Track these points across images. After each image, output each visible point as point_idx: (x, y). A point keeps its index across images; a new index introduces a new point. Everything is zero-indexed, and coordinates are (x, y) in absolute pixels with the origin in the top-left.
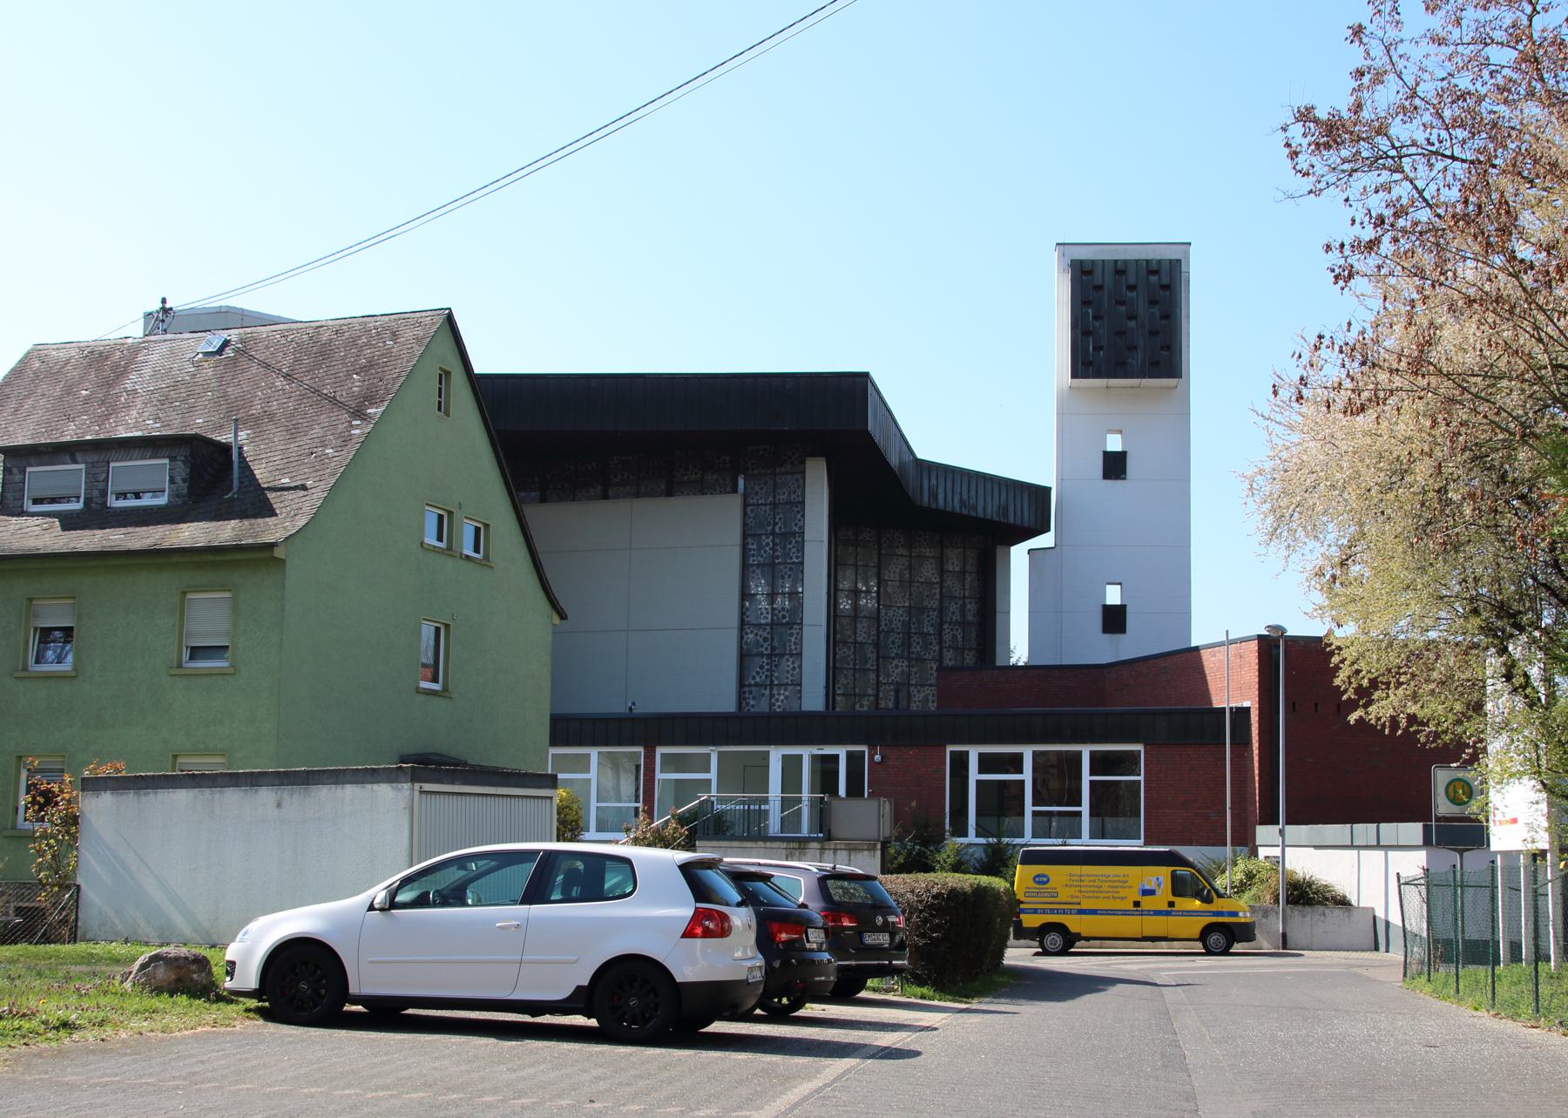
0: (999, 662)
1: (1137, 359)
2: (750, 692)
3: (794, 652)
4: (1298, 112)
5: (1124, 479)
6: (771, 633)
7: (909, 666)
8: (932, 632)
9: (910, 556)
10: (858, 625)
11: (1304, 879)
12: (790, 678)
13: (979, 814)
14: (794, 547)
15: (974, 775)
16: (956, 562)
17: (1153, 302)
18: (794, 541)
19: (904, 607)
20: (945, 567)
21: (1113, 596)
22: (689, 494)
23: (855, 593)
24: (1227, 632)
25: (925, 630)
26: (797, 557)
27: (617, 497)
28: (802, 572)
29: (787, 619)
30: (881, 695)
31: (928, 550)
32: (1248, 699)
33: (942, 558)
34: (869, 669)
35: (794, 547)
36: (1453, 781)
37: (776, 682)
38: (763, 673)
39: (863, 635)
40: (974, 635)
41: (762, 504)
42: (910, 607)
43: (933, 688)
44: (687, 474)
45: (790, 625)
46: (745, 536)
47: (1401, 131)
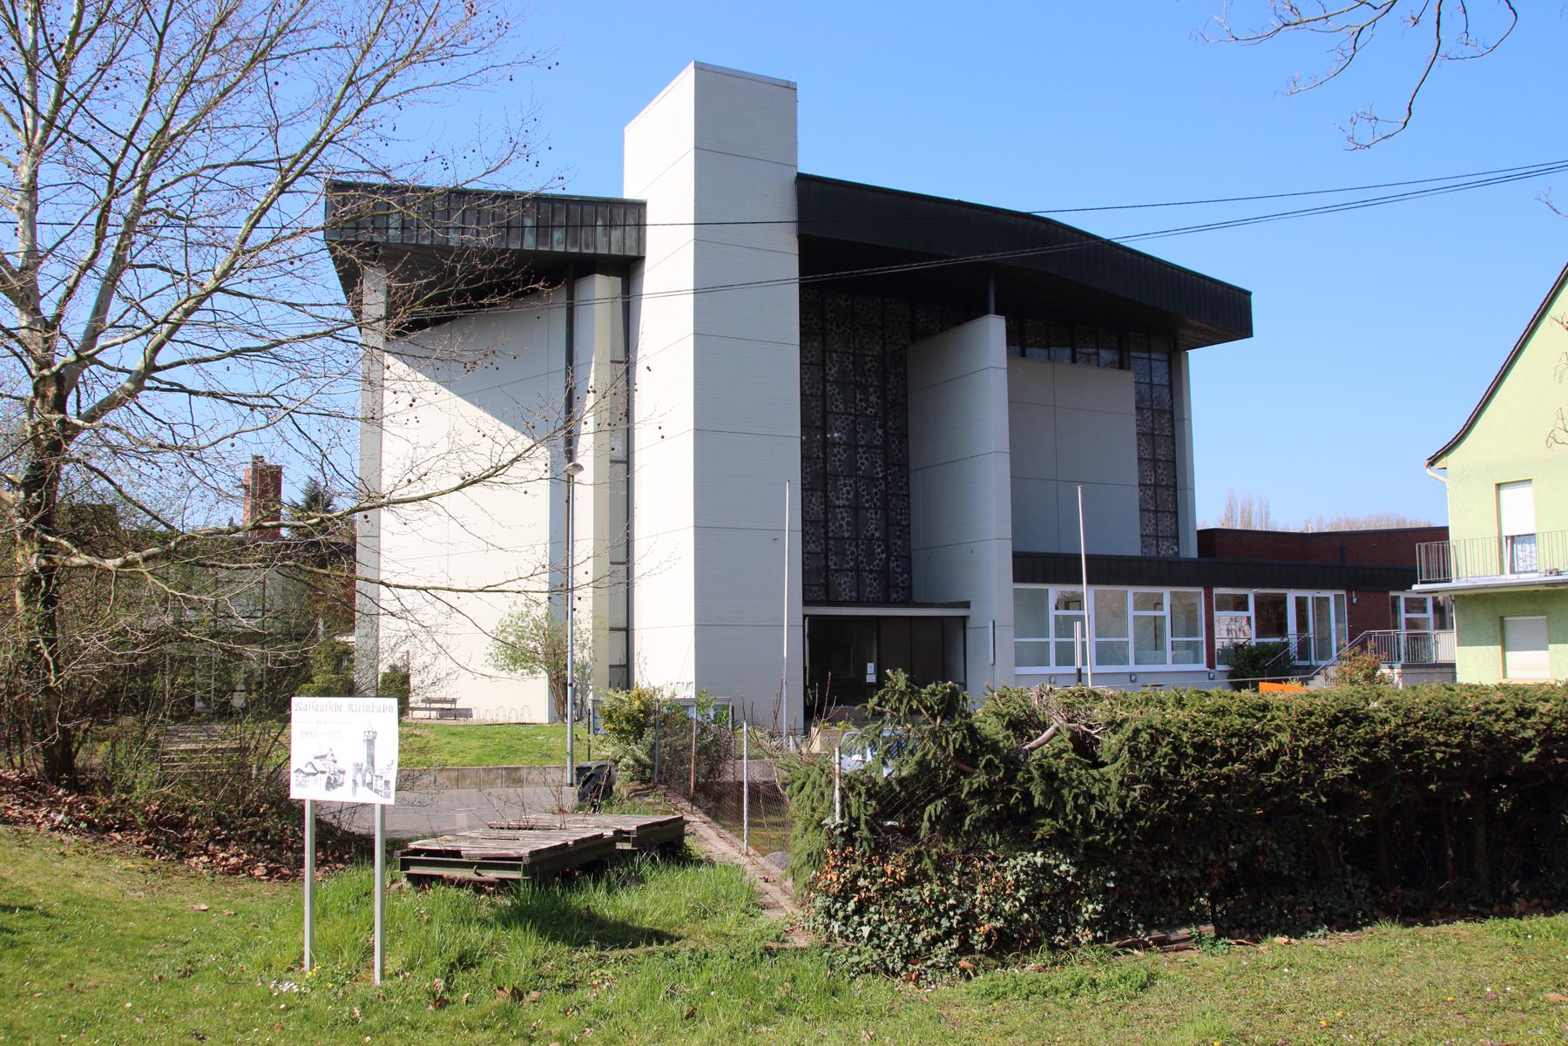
1: (804, 323)
6: (1155, 492)
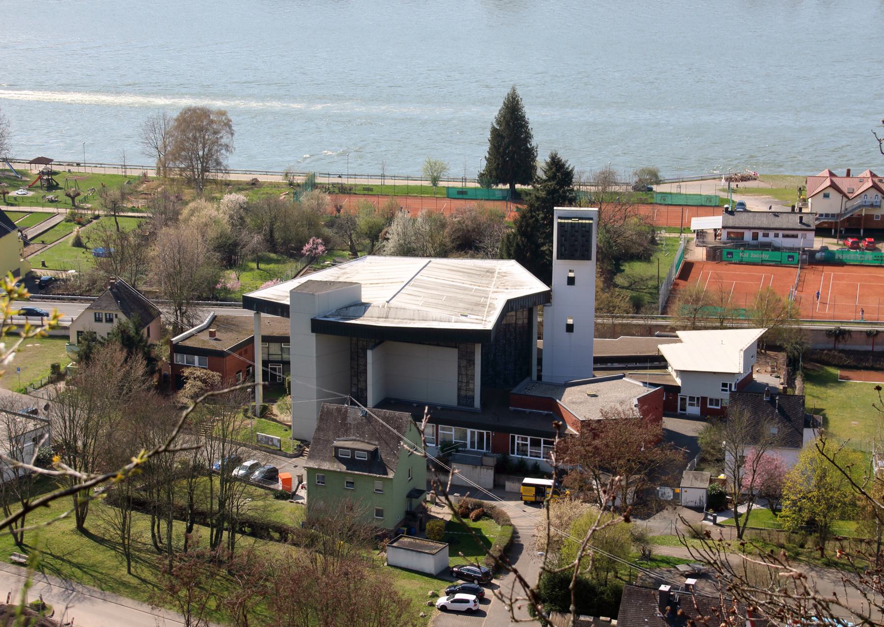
17: (583, 236)
21: (570, 321)
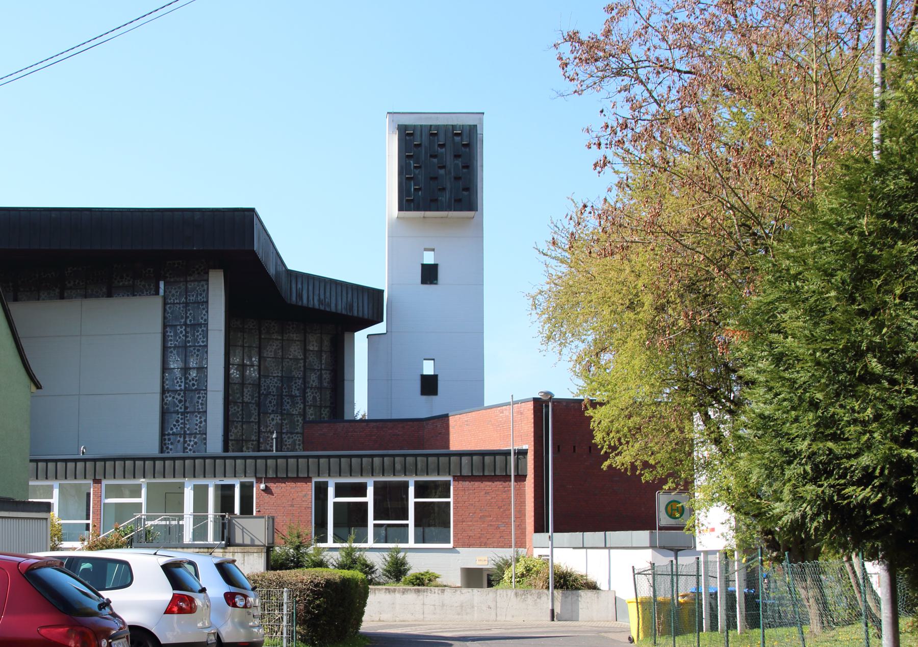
0: (347, 417)
2: (169, 439)
3: (201, 410)
4: (568, 35)
5: (436, 284)
6: (185, 396)
7: (281, 420)
8: (298, 395)
9: (282, 340)
10: (245, 390)
11: (567, 572)
12: (198, 429)
13: (336, 525)
14: (200, 334)
15: (332, 499)
16: (315, 344)
18: (200, 330)
19: (277, 376)
20: (307, 348)
21: (428, 369)
22: (123, 296)
23: (242, 367)
24: (512, 396)
25: (293, 393)
26: (203, 342)
27: (70, 297)
28: (207, 352)
29: (196, 386)
30: (261, 440)
31: (295, 335)
32: (526, 444)
33: (305, 340)
34: (252, 422)
35: (200, 334)
36: (671, 502)
37: (188, 432)
38: (179, 425)
39: (249, 397)
40: (328, 396)
41: (177, 303)
42: (282, 377)
43: (299, 435)
44: (122, 281)
45: (198, 390)
46: (165, 326)
47: (637, 51)
